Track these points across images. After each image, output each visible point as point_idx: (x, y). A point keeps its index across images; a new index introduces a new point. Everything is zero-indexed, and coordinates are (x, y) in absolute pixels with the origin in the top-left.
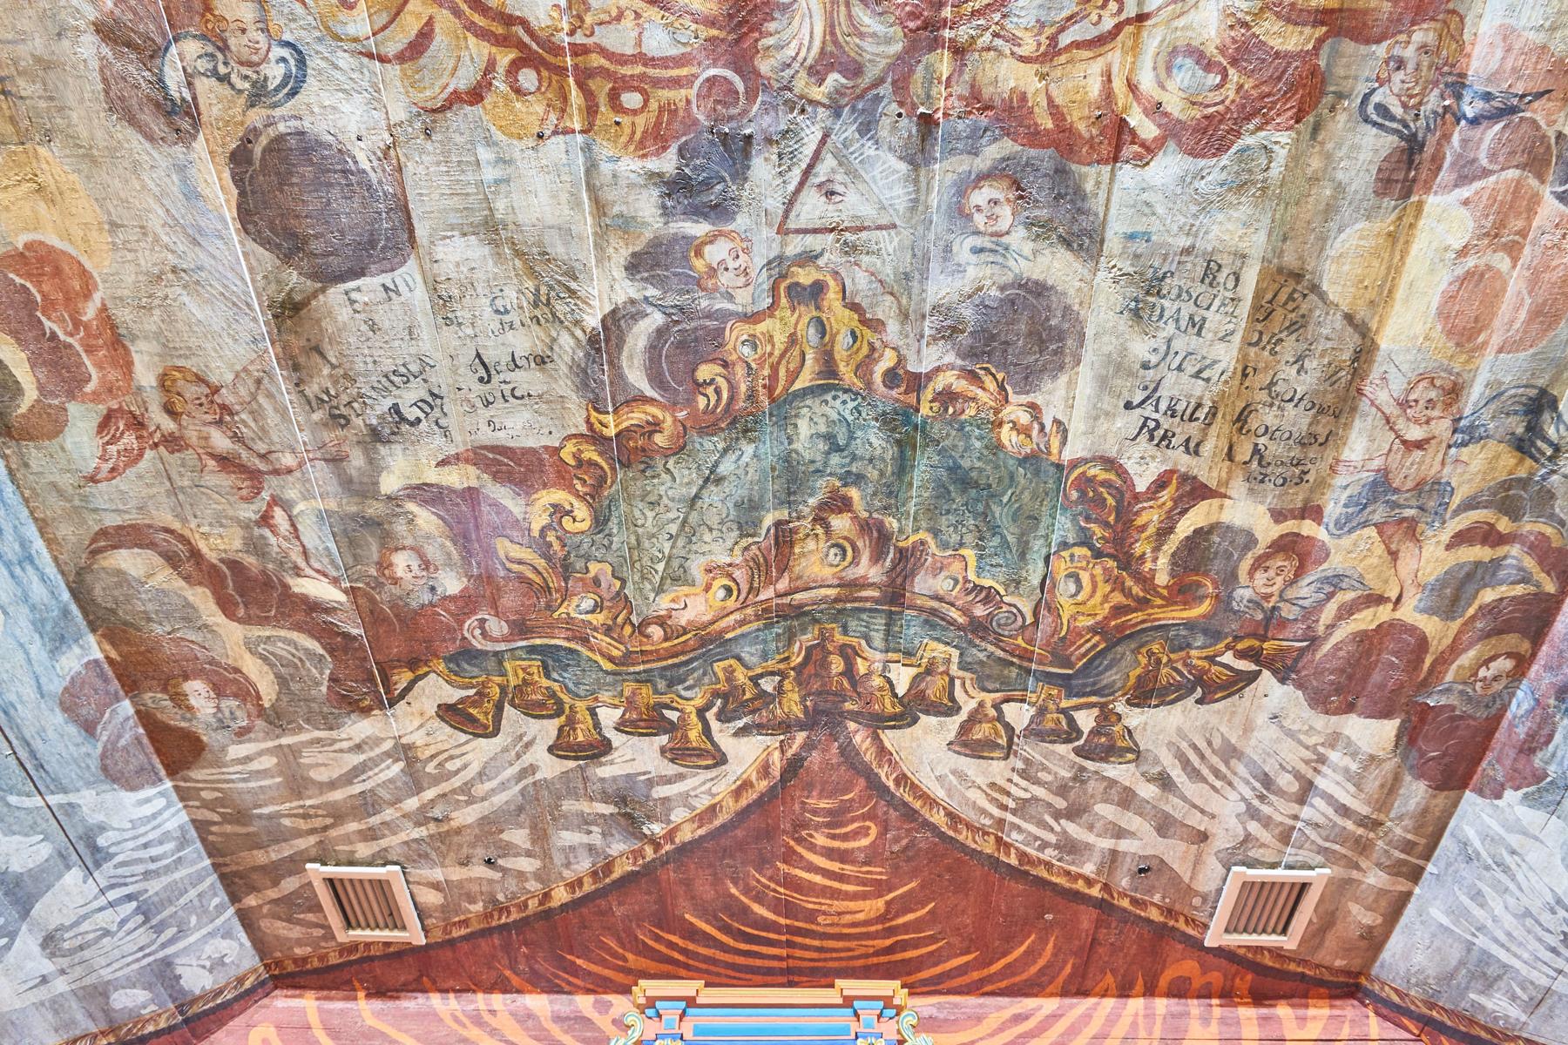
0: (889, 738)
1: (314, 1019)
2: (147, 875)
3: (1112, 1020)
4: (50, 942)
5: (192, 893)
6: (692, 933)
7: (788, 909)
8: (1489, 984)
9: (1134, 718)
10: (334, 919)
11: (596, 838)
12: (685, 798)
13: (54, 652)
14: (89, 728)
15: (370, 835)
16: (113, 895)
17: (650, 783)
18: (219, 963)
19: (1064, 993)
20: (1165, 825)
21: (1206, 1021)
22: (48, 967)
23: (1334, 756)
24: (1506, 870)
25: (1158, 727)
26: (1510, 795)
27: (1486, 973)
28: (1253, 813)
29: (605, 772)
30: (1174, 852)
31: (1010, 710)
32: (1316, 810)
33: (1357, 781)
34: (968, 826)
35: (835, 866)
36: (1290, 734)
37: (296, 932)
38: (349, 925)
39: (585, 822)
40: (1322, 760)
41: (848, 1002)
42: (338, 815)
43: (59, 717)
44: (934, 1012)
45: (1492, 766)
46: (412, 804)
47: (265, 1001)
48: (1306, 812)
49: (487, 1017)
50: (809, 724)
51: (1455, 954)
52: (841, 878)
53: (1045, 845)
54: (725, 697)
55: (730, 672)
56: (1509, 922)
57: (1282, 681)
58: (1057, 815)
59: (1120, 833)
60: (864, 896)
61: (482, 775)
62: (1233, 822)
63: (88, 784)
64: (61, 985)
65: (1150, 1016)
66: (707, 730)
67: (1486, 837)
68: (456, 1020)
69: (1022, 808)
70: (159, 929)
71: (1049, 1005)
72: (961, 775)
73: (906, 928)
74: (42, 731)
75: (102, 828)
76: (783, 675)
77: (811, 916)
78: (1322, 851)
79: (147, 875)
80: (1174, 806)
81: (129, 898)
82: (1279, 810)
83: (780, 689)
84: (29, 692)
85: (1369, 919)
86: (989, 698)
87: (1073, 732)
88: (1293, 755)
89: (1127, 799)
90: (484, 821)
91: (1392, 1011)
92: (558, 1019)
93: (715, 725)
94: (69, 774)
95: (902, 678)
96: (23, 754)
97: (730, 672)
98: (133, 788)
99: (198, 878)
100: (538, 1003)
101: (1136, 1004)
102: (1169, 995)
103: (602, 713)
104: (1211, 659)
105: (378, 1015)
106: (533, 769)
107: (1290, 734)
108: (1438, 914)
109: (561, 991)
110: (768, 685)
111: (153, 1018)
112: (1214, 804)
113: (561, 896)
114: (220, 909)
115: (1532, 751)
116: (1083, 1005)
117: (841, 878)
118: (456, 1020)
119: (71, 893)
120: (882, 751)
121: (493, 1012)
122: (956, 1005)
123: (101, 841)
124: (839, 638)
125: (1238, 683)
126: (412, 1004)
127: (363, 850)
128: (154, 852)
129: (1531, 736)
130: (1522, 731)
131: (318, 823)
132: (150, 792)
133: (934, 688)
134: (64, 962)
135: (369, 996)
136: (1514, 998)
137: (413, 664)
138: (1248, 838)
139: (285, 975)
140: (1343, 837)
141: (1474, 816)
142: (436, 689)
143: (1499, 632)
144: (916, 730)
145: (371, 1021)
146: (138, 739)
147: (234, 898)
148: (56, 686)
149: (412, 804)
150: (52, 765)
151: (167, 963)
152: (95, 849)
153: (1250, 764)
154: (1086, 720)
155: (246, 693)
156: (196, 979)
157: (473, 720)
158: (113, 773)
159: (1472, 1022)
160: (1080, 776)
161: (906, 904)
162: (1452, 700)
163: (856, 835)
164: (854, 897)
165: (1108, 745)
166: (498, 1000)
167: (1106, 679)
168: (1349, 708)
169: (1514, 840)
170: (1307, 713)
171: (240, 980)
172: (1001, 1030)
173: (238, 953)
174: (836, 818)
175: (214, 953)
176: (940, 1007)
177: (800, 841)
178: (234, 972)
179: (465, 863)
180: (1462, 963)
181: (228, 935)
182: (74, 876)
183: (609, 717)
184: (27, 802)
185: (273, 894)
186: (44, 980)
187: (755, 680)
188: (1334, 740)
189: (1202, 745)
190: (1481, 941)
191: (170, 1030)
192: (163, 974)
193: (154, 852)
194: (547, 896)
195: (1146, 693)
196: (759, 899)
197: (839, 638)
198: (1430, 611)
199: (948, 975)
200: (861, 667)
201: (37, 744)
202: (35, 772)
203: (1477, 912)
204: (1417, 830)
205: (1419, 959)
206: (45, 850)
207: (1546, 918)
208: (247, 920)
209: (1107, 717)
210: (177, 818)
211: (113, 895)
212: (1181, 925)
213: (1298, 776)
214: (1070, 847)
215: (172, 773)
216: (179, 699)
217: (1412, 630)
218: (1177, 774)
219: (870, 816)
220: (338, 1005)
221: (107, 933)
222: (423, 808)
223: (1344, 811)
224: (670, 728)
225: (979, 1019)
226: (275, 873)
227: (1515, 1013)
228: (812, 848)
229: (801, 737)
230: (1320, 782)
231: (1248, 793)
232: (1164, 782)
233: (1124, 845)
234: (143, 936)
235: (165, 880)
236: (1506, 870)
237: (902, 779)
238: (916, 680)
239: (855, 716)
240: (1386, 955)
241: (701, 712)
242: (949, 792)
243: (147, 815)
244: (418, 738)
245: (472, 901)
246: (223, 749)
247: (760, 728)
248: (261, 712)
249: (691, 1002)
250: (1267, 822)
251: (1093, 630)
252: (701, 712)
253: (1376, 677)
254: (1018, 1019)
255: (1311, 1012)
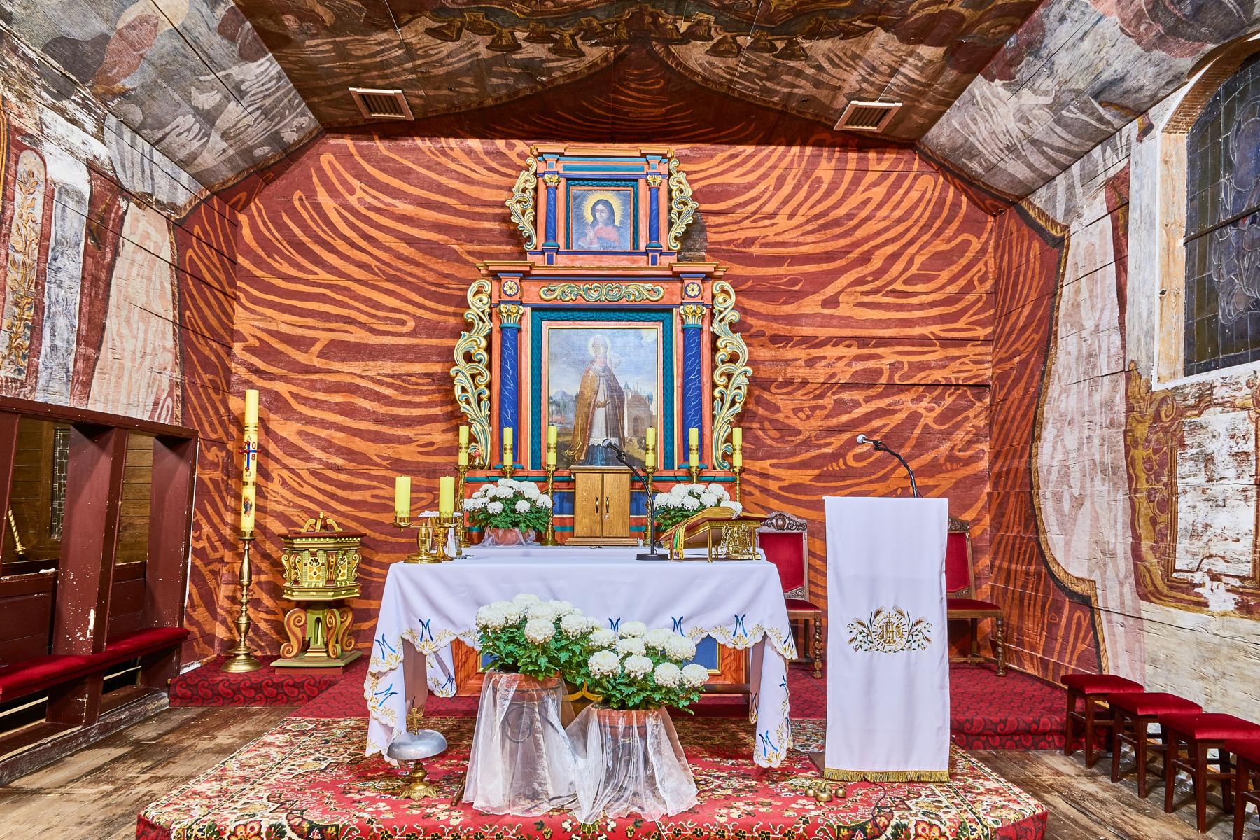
0: (673, 49)
1: (353, 150)
2: (264, 97)
3: (781, 158)
4: (225, 136)
5: (286, 100)
6: (561, 118)
7: (614, 110)
8: (971, 158)
9: (806, 44)
10: (364, 110)
11: (511, 81)
12: (560, 69)
13: (212, 10)
14: (232, 39)
15: (386, 77)
16: (250, 109)
17: (542, 62)
18: (300, 128)
19: (758, 144)
20: (817, 84)
21: (830, 160)
22: (225, 145)
23: (911, 60)
24: (989, 112)
25: (820, 48)
26: (997, 81)
27: (972, 153)
28: (864, 80)
29: (518, 56)
30: (822, 94)
31: (740, 40)
32: (898, 80)
33: (922, 70)
34: (713, 82)
35: (641, 96)
36: (887, 51)
37: (341, 112)
38: (371, 111)
39: (504, 76)
40: (905, 61)
41: (644, 156)
42: (367, 68)
43: (218, 38)
44: (688, 152)
45: (993, 67)
46: (409, 65)
47: (324, 140)
48: (893, 81)
49: (449, 151)
50: (631, 41)
51: (960, 141)
52: (644, 100)
53: (753, 90)
54: (586, 31)
55: (589, 22)
56: (985, 133)
57: (886, 31)
58: (761, 79)
59: (794, 86)
60: (655, 107)
61: (448, 56)
62: (854, 83)
63: (235, 64)
64: (231, 152)
65: (801, 156)
66: (575, 43)
67: (983, 97)
68: (432, 152)
69: (742, 76)
70: (272, 120)
71: (750, 149)
72: (711, 64)
73: (676, 119)
74: (211, 46)
75: (243, 82)
76: (618, 23)
77: (627, 114)
78: (898, 95)
79: (264, 97)
80: (824, 78)
81: (257, 109)
82: (879, 80)
83: (616, 29)
84: (204, 30)
85: (921, 121)
86: (729, 35)
87: (774, 48)
88: (887, 58)
89: (799, 73)
90: (448, 74)
91: (928, 158)
92: (487, 153)
93: (579, 42)
94: (226, 61)
95: (683, 26)
96: (204, 58)
97: (589, 22)
98: (254, 61)
99: (289, 92)
100: (475, 143)
101: (795, 150)
102: (813, 145)
103: (517, 34)
104: (850, 23)
105: (388, 148)
106: (477, 54)
107: (887, 51)
108: (955, 123)
109: (486, 138)
110: (609, 27)
111: (273, 157)
112: (845, 76)
113: (490, 102)
114: (299, 105)
115: (1011, 66)
116: (767, 150)
117: (644, 100)
118: (432, 152)
119: (233, 110)
120: (670, 54)
121: (452, 149)
122: (700, 149)
123: (243, 87)
124: (650, 9)
125: (862, 32)
126: (406, 143)
127: (380, 82)
128: (267, 86)
129: (1012, 59)
130: (1009, 55)
131: (355, 71)
132: (262, 60)
133: (700, 31)
134: (231, 142)
135: (381, 138)
136: (981, 165)
137: (412, 12)
138: (861, 89)
139: (329, 128)
140: (912, 90)
141: (980, 87)
142: (425, 22)
143: (1003, 16)
144: (690, 46)
145: (385, 152)
146: (255, 38)
147: (304, 98)
148: (216, 24)
149: (409, 65)
150: (218, 60)
151: (277, 132)
152: (240, 91)
153: (866, 62)
154: (780, 45)
155: (317, 19)
156: (290, 136)
157: (445, 35)
158: (247, 56)
159: (961, 170)
160: (775, 65)
161: (676, 110)
162: (975, 40)
163: (653, 84)
164: (650, 107)
165: (792, 52)
166: (453, 142)
167: (793, 29)
168: (921, 42)
169: (995, 101)
170: (898, 43)
171: (310, 133)
172: (722, 163)
173: (306, 120)
174: (642, 78)
175: (297, 123)
176: (691, 149)
177: (622, 85)
178: (307, 131)
179: (438, 89)
180: (962, 146)
181: (303, 114)
182: (232, 104)
183: (520, 35)
184: (208, 78)
185: (329, 98)
186: (224, 151)
187: (603, 26)
188: (911, 54)
189: (841, 54)
190: (972, 139)
191: (280, 161)
192: (275, 138)
193: (267, 86)
194: (482, 102)
195: (811, 35)
196: (599, 107)
197: (650, 9)
198: (967, 7)
199: (698, 135)
200: (661, 20)
201: (211, 52)
202: (211, 64)
203: (973, 126)
204: (950, 88)
205: (943, 139)
206: (218, 97)
207: (1001, 136)
208: (312, 107)
209: (791, 43)
210: (276, 69)
211: (250, 109)
212: (823, 120)
213: (890, 67)
214: (765, 90)
215: (271, 50)
216: (280, 23)
217: (958, 14)
218: (826, 65)
219: (662, 77)
220: (365, 143)
221: (249, 126)
222: (415, 67)
223: (913, 81)
224: (554, 41)
225: (712, 157)
226: (329, 90)
227: (980, 170)
228: (630, 89)
229: (625, 47)
230: (902, 70)
231: (863, 73)
232: (820, 68)
233: (796, 91)
234: (265, 124)
235: (273, 97)
236: (989, 112)
237: (679, 64)
238: (689, 27)
239: (655, 39)
240: (934, 130)
241: (572, 36)
242: (704, 70)
243: (262, 71)
244: (414, 41)
245: (441, 103)
246: (303, 42)
247: (604, 44)
248: (325, 27)
249: (561, 154)
250: (872, 84)
251: (788, 11)
252: (572, 36)
253: (937, 31)
254: (732, 157)
255: (886, 156)
